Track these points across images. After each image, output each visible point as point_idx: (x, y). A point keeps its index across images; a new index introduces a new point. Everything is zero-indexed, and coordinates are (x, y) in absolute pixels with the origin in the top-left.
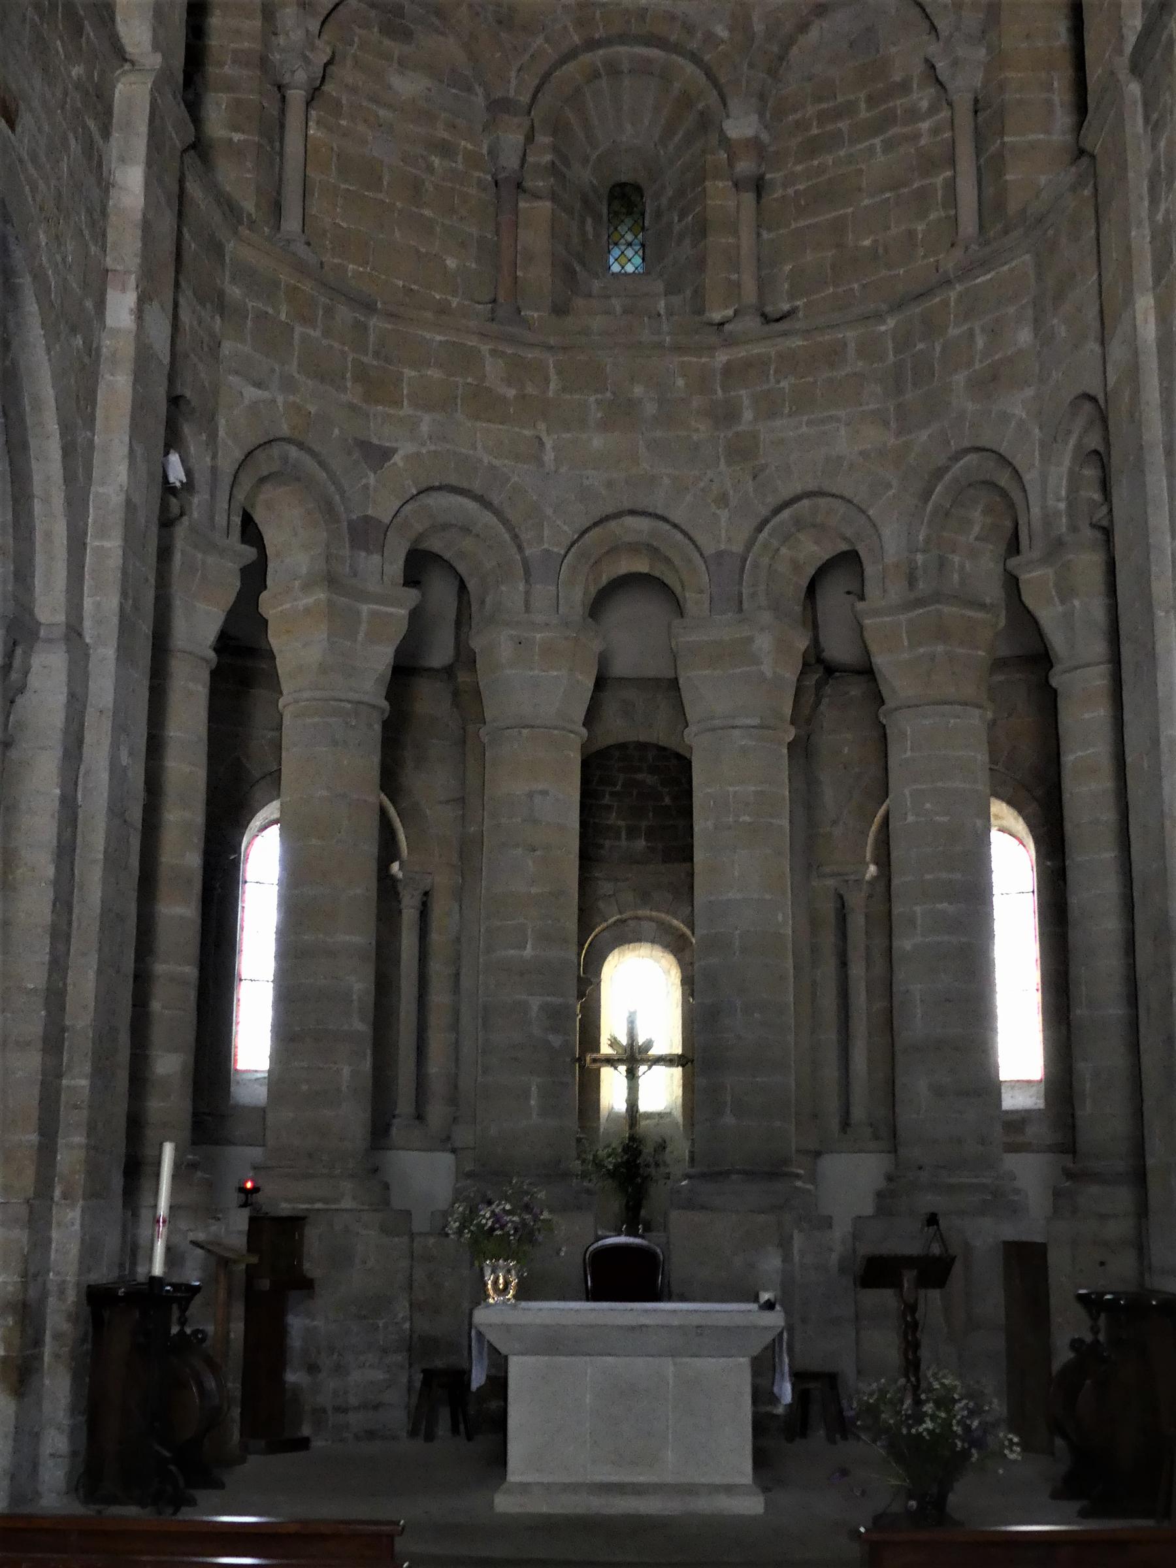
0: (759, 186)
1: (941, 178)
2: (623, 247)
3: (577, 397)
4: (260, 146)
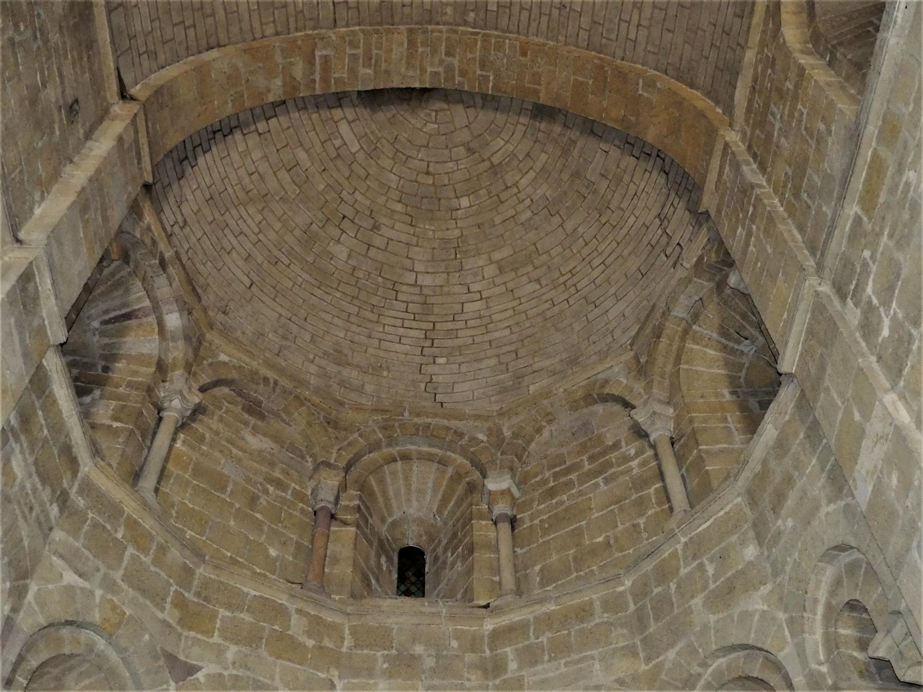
0: (513, 522)
1: (653, 489)
2: (408, 585)
3: (365, 651)
4: (132, 432)
